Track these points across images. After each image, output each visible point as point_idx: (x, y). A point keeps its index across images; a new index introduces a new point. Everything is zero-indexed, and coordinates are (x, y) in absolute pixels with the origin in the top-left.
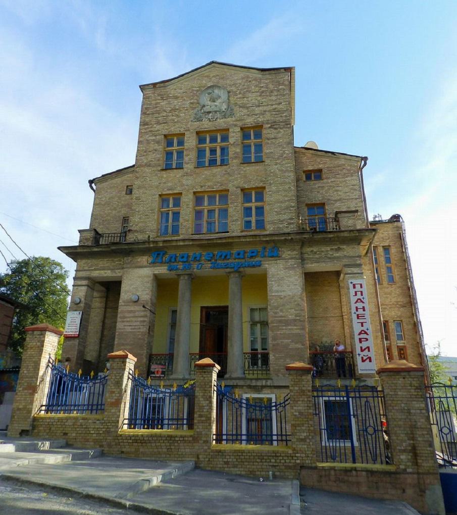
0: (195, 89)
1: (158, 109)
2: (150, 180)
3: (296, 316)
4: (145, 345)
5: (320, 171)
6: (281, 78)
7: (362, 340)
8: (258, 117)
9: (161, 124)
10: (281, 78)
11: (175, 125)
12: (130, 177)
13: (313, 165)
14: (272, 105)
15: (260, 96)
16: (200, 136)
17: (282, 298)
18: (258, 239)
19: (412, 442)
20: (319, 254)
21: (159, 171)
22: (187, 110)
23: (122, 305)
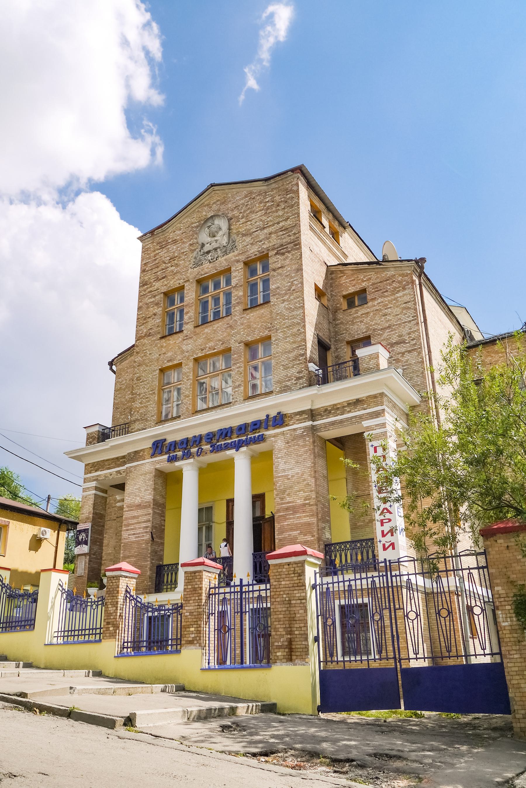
0: (195, 225)
1: (157, 262)
3: (305, 500)
4: (149, 555)
5: (364, 291)
6: (289, 184)
7: (384, 521)
8: (263, 244)
9: (161, 279)
10: (289, 184)
13: (354, 286)
14: (278, 223)
16: (201, 283)
17: (289, 479)
19: (289, 636)
21: (159, 340)
23: (126, 511)
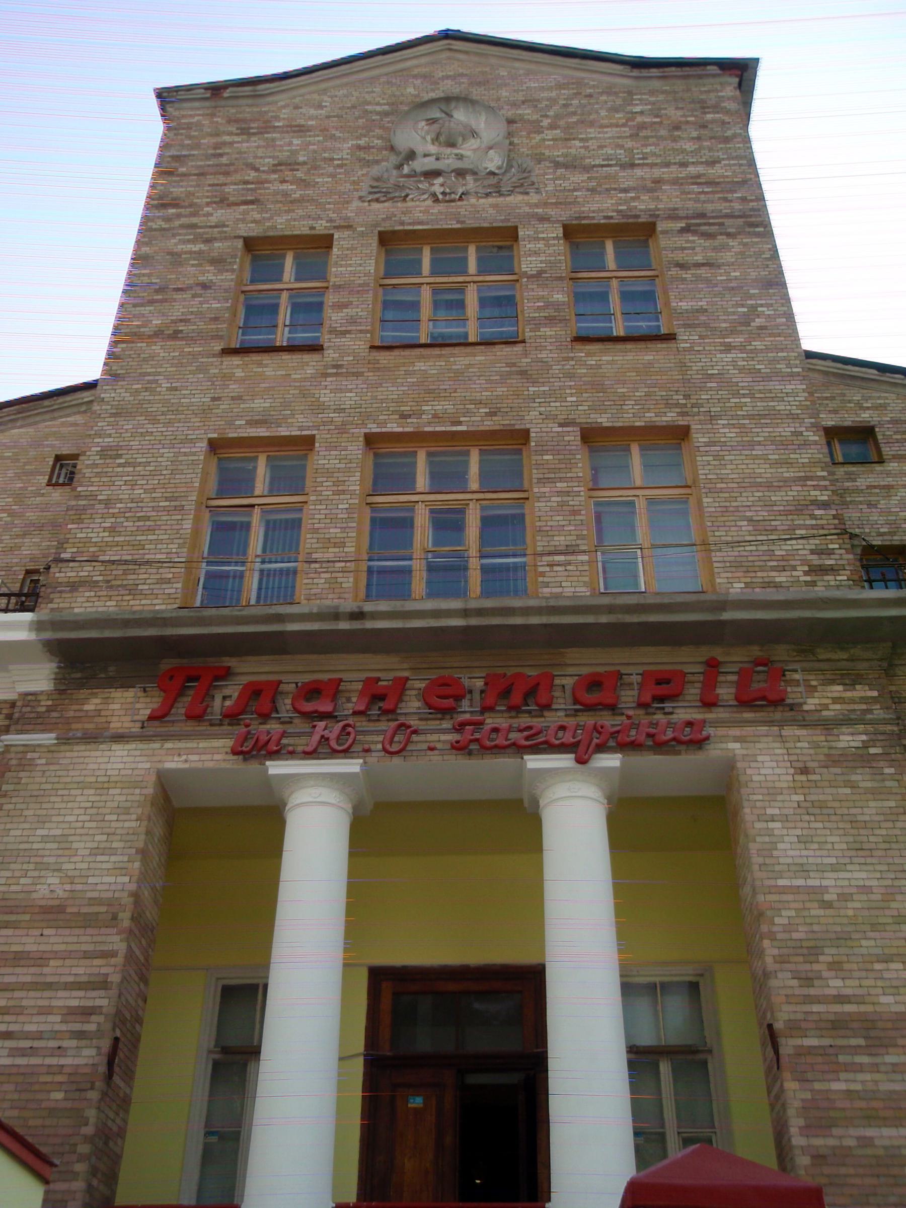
1: (224, 160)
11: (288, 212)
17: (828, 905)
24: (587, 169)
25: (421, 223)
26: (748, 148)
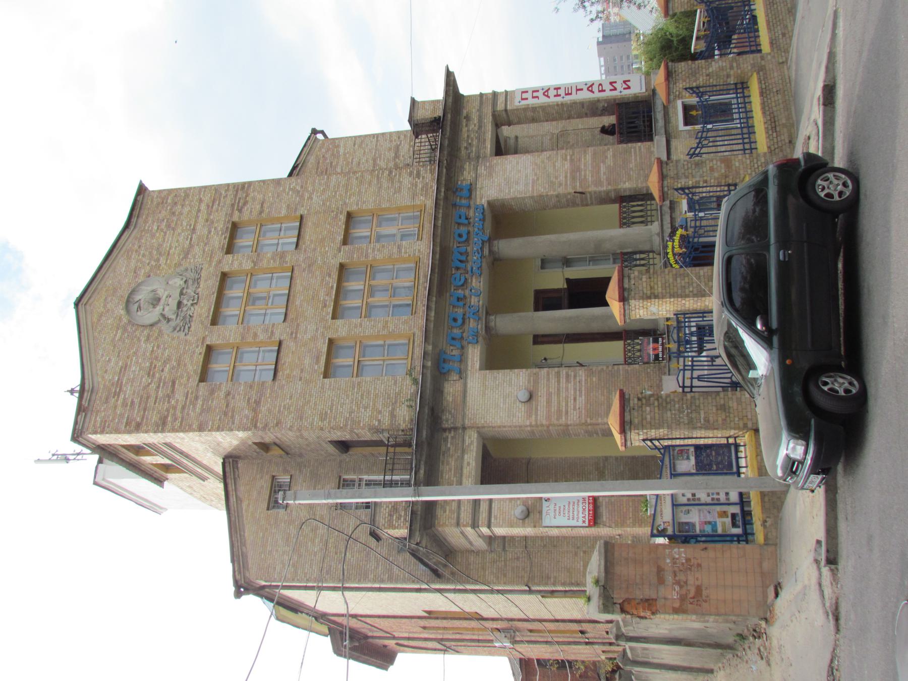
1: (137, 401)
2: (291, 398)
3: (566, 160)
11: (185, 365)
12: (249, 504)
14: (199, 211)
15: (174, 229)
17: (538, 179)
18: (442, 203)
20: (472, 140)
22: (158, 347)
24: (191, 246)
25: (210, 310)
26: (187, 195)
